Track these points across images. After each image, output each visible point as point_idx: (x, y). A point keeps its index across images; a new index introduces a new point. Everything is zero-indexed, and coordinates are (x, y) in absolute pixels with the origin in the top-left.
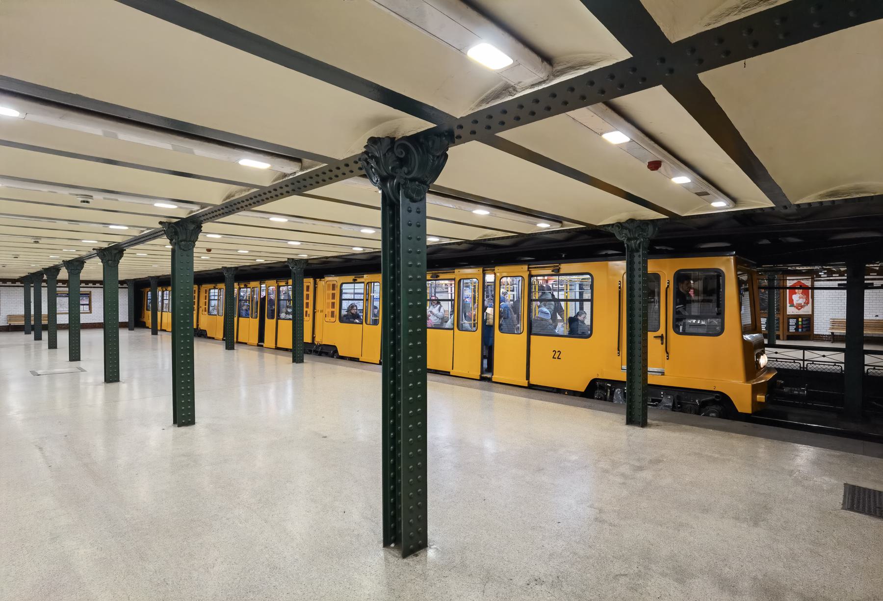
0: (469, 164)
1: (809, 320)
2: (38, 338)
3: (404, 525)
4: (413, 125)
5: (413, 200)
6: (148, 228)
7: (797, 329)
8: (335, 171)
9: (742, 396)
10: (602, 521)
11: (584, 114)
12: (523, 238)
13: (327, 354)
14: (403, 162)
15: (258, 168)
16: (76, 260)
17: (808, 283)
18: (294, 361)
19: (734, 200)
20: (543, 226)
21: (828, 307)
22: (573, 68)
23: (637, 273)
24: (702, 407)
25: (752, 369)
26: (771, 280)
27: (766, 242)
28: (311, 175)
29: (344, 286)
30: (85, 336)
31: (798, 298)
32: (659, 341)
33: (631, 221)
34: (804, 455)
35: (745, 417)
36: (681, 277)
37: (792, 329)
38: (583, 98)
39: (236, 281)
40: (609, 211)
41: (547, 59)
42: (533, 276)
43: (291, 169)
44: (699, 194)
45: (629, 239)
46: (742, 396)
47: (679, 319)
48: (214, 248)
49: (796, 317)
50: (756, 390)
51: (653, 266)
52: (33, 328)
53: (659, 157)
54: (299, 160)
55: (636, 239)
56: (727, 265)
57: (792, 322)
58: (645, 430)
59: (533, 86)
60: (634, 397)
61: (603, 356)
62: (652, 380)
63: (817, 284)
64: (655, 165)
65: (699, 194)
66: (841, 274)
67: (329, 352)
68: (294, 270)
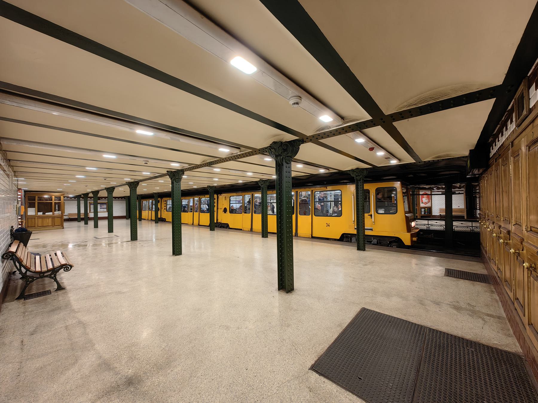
0: (307, 151)
1: (430, 209)
2: (86, 223)
3: (285, 283)
4: (290, 137)
5: (287, 163)
6: (158, 173)
7: (425, 213)
8: (254, 152)
9: (406, 239)
10: (356, 281)
11: (351, 134)
12: (312, 176)
13: (224, 227)
14: (285, 150)
15: (224, 151)
16: (112, 187)
17: (429, 193)
18: (211, 230)
19: (399, 160)
20: (322, 171)
21: (438, 203)
22: (351, 121)
23: (359, 189)
24: (391, 243)
25: (409, 228)
26: (413, 192)
27: (412, 176)
28: (243, 152)
29: (231, 198)
30: (100, 223)
31: (425, 199)
32: (370, 217)
33: (357, 169)
34: (431, 260)
35: (408, 247)
36: (378, 191)
37: (423, 213)
38: (353, 130)
39: (159, 197)
40: (347, 164)
41: (342, 118)
42: (184, 209)
43: (236, 152)
44: (386, 158)
45: (356, 176)
46: (406, 239)
47: (377, 207)
48: (189, 181)
49: (424, 208)
50: (412, 236)
51: (366, 186)
52: (82, 219)
53: (374, 146)
54: (239, 148)
55: (359, 176)
56: (398, 185)
57: (423, 210)
58: (364, 252)
59: (337, 126)
60: (360, 239)
61: (346, 223)
62: (367, 233)
63: (433, 193)
64: (371, 149)
65: (386, 158)
66: (443, 188)
67: (225, 226)
68: (262, 186)
